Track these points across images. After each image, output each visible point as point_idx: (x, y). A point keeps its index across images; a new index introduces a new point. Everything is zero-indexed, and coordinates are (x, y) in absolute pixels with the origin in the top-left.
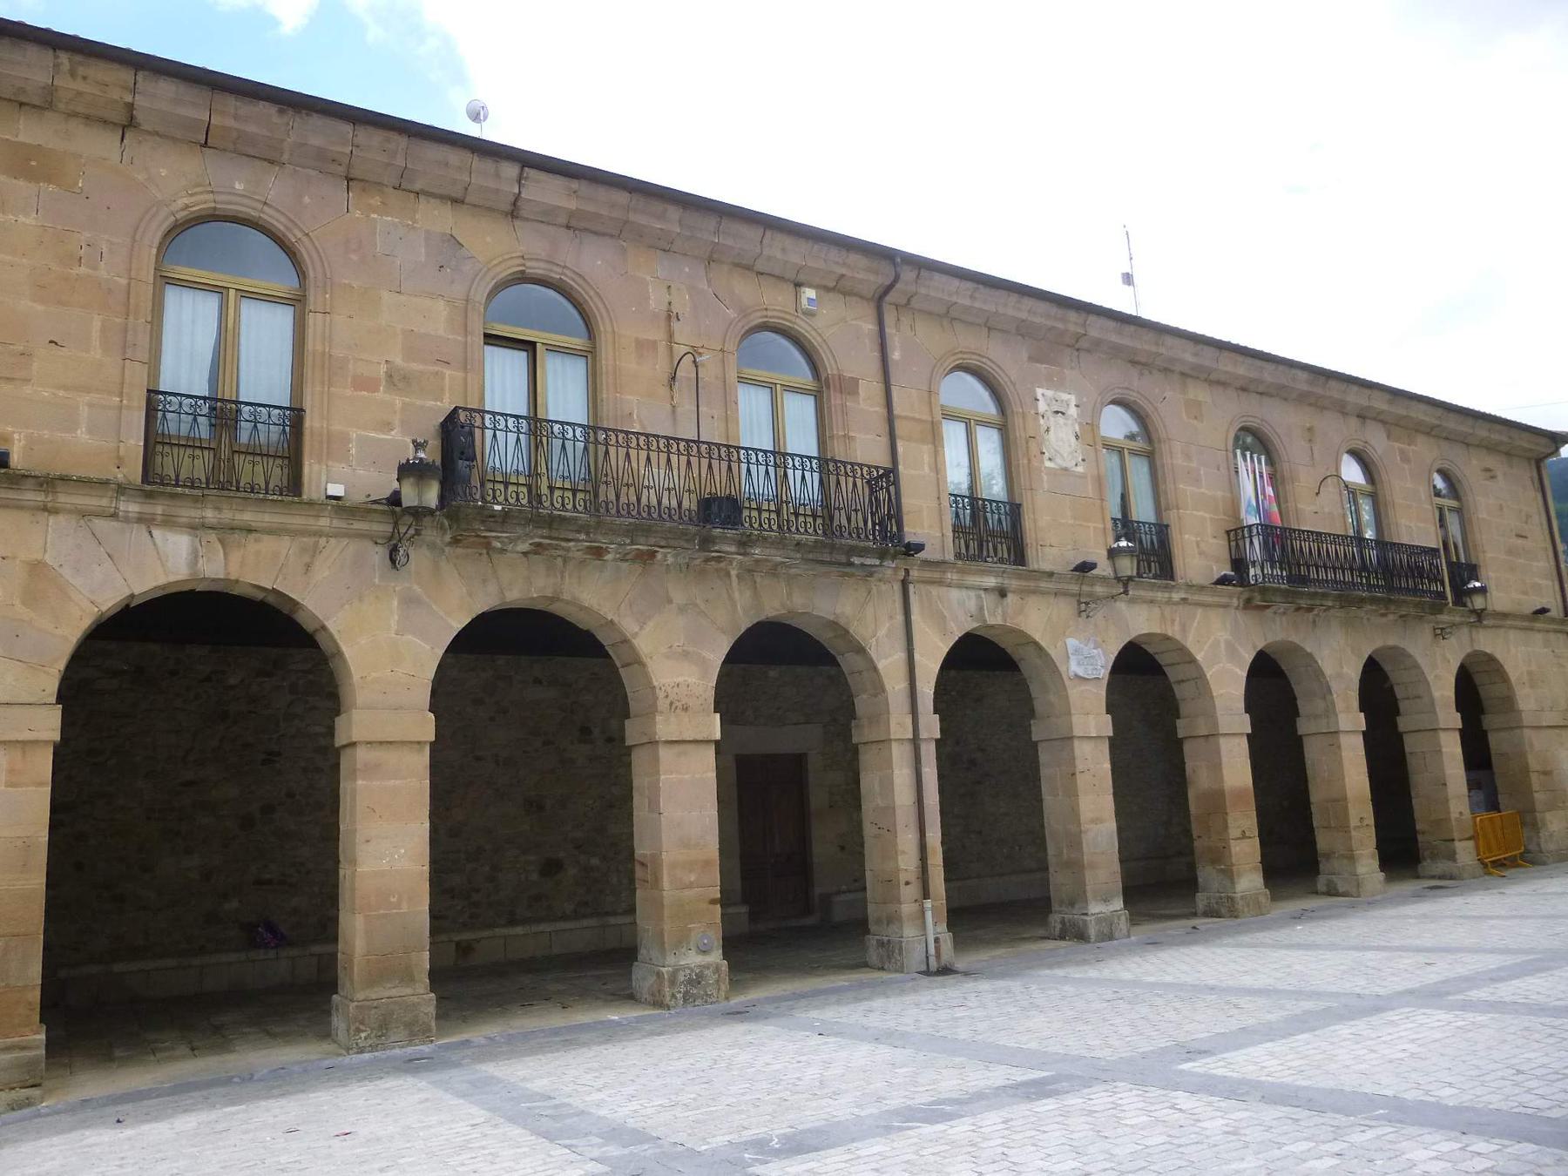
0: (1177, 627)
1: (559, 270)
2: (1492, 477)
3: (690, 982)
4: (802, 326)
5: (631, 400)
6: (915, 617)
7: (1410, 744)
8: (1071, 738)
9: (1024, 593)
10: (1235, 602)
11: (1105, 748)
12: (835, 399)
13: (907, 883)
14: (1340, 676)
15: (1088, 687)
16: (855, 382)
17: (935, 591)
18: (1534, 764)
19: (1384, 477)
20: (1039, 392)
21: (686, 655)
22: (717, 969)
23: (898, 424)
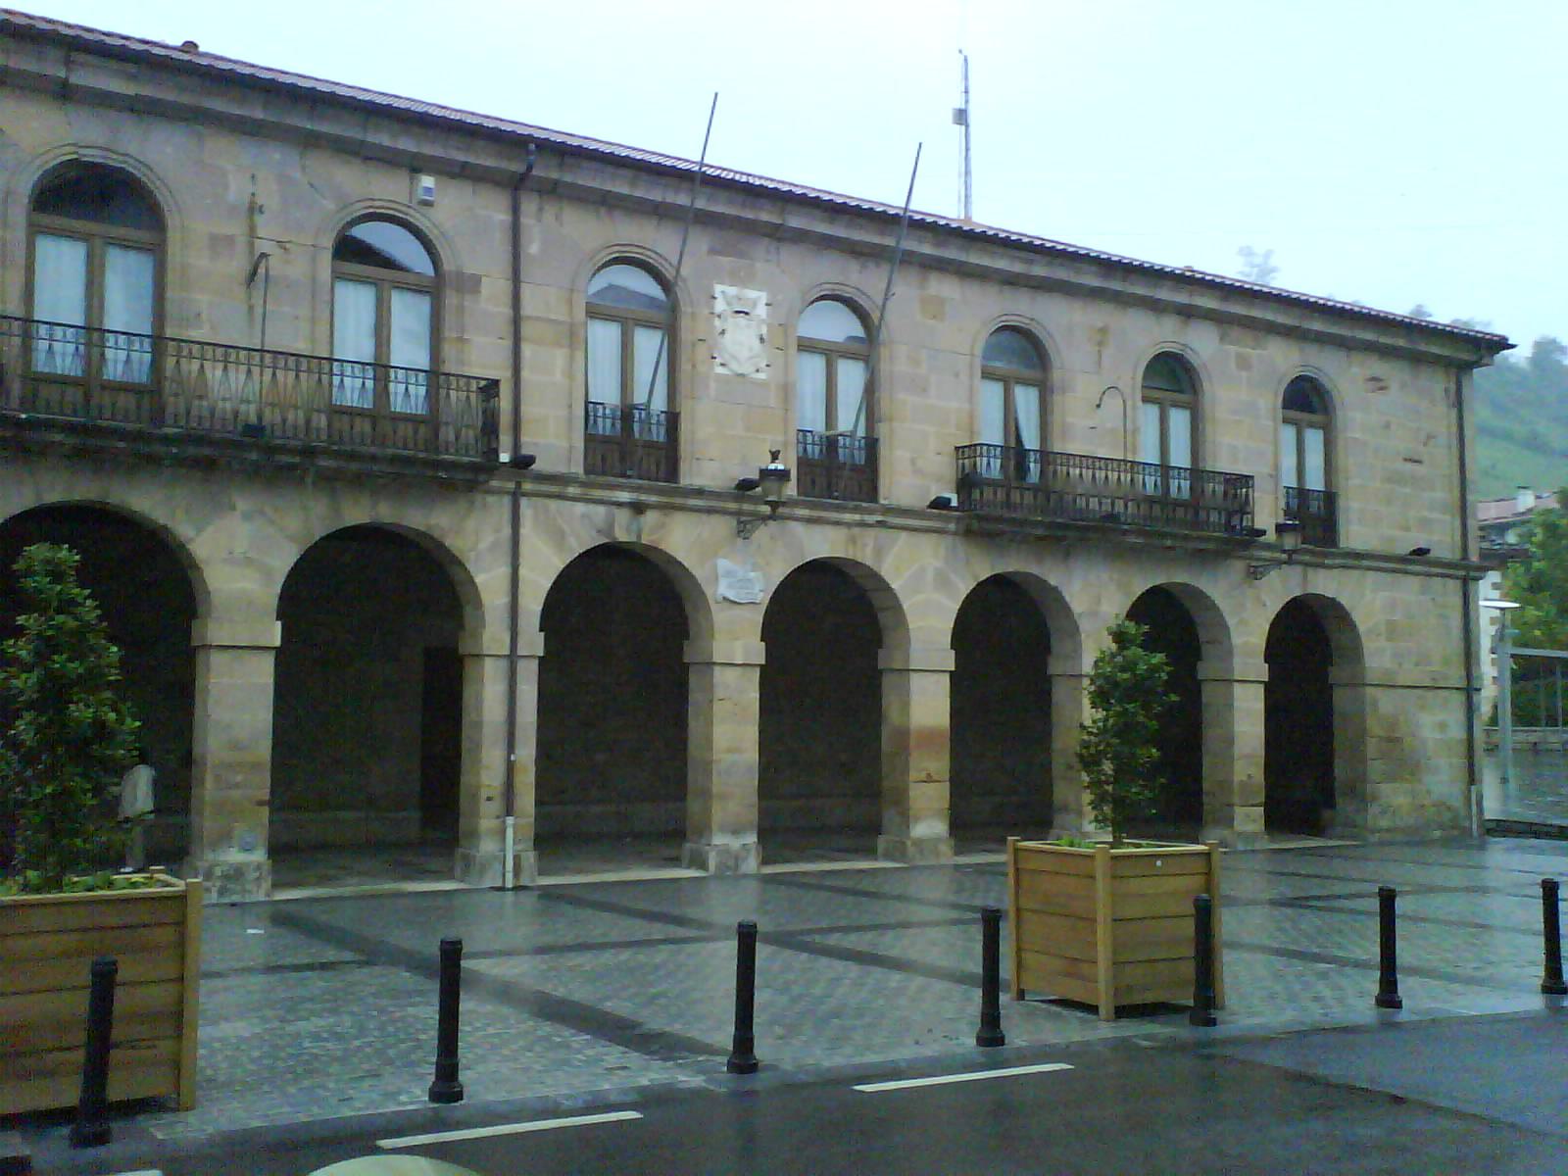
0: (869, 551)
1: (121, 158)
2: (1382, 389)
3: (226, 877)
4: (417, 218)
5: (202, 300)
6: (526, 530)
7: (1208, 693)
8: (1231, 681)
9: (667, 508)
10: (952, 526)
11: (755, 675)
12: (451, 299)
13: (489, 799)
14: (1094, 614)
15: (737, 611)
16: (476, 281)
17: (553, 505)
18: (1374, 727)
19: (1206, 385)
20: (718, 289)
21: (248, 561)
22: (259, 867)
23: (526, 329)
